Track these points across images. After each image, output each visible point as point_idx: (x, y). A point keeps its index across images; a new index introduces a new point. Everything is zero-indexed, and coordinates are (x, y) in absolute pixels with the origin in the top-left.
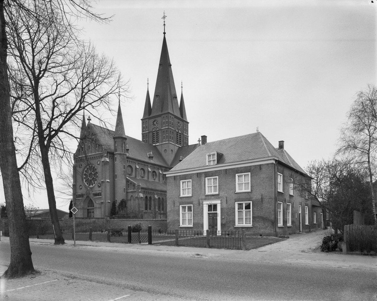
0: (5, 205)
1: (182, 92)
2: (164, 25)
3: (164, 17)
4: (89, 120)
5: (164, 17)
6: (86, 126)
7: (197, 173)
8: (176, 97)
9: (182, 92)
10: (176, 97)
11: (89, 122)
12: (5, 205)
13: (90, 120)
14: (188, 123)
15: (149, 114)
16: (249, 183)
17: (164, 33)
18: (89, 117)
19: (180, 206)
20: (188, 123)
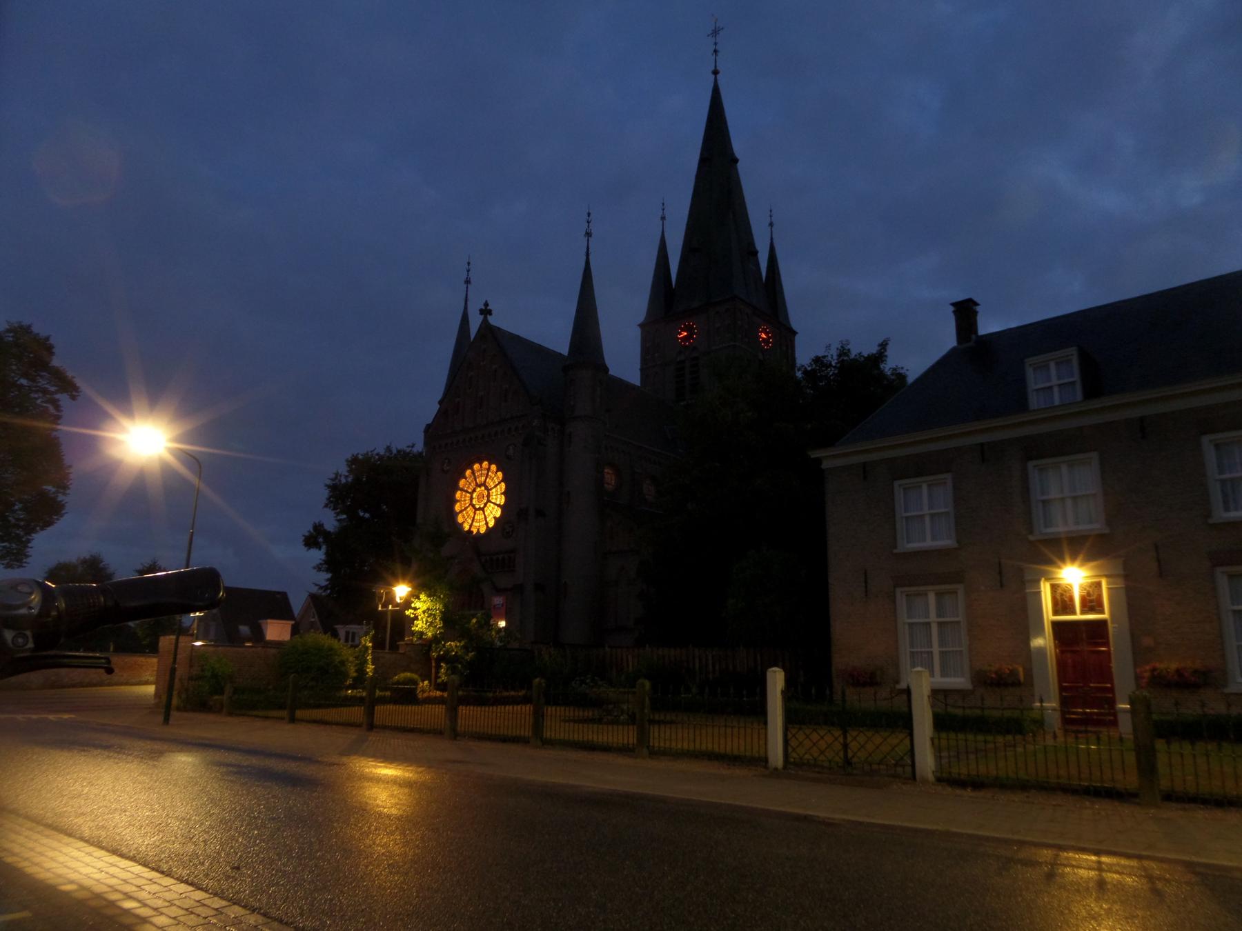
0: (911, 379)
1: (588, 255)
2: (716, 51)
3: (715, 32)
4: (486, 312)
5: (715, 32)
6: (472, 337)
7: (982, 445)
8: (754, 253)
9: (588, 255)
10: (755, 253)
11: (485, 321)
12: (911, 379)
13: (490, 312)
14: (795, 333)
15: (669, 300)
16: (928, 624)
17: (716, 73)
18: (486, 304)
19: (898, 590)
20: (795, 333)
